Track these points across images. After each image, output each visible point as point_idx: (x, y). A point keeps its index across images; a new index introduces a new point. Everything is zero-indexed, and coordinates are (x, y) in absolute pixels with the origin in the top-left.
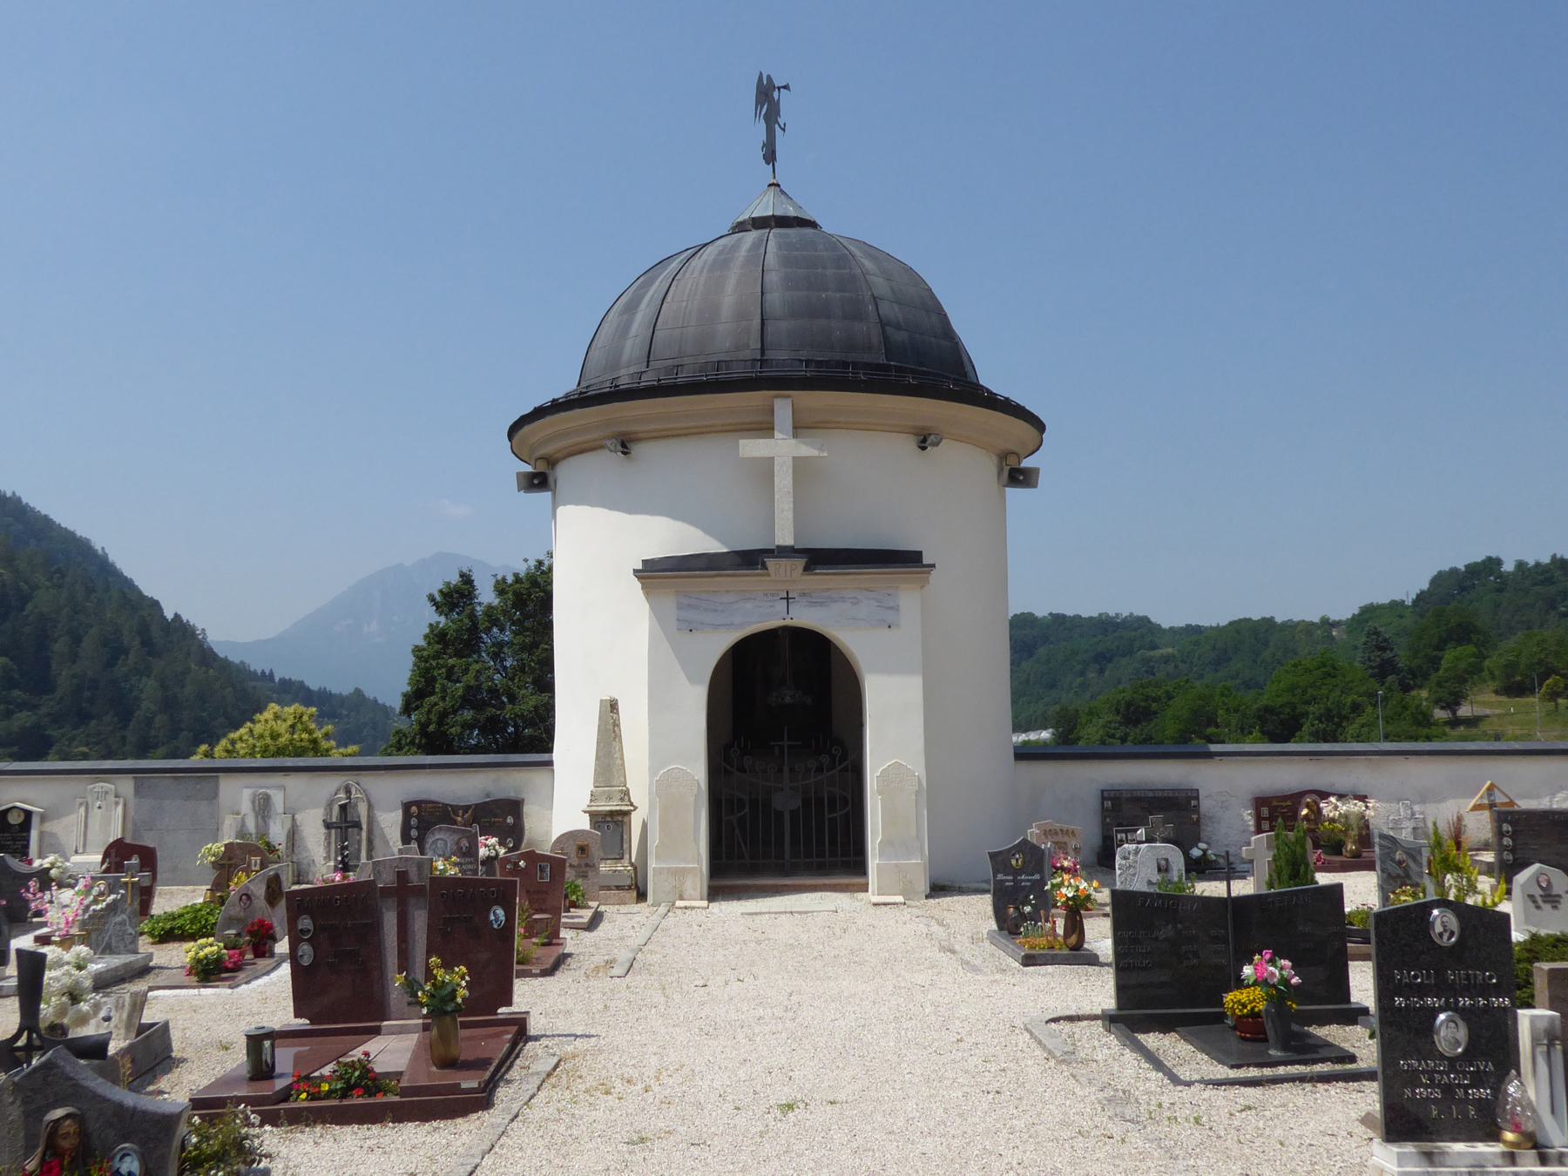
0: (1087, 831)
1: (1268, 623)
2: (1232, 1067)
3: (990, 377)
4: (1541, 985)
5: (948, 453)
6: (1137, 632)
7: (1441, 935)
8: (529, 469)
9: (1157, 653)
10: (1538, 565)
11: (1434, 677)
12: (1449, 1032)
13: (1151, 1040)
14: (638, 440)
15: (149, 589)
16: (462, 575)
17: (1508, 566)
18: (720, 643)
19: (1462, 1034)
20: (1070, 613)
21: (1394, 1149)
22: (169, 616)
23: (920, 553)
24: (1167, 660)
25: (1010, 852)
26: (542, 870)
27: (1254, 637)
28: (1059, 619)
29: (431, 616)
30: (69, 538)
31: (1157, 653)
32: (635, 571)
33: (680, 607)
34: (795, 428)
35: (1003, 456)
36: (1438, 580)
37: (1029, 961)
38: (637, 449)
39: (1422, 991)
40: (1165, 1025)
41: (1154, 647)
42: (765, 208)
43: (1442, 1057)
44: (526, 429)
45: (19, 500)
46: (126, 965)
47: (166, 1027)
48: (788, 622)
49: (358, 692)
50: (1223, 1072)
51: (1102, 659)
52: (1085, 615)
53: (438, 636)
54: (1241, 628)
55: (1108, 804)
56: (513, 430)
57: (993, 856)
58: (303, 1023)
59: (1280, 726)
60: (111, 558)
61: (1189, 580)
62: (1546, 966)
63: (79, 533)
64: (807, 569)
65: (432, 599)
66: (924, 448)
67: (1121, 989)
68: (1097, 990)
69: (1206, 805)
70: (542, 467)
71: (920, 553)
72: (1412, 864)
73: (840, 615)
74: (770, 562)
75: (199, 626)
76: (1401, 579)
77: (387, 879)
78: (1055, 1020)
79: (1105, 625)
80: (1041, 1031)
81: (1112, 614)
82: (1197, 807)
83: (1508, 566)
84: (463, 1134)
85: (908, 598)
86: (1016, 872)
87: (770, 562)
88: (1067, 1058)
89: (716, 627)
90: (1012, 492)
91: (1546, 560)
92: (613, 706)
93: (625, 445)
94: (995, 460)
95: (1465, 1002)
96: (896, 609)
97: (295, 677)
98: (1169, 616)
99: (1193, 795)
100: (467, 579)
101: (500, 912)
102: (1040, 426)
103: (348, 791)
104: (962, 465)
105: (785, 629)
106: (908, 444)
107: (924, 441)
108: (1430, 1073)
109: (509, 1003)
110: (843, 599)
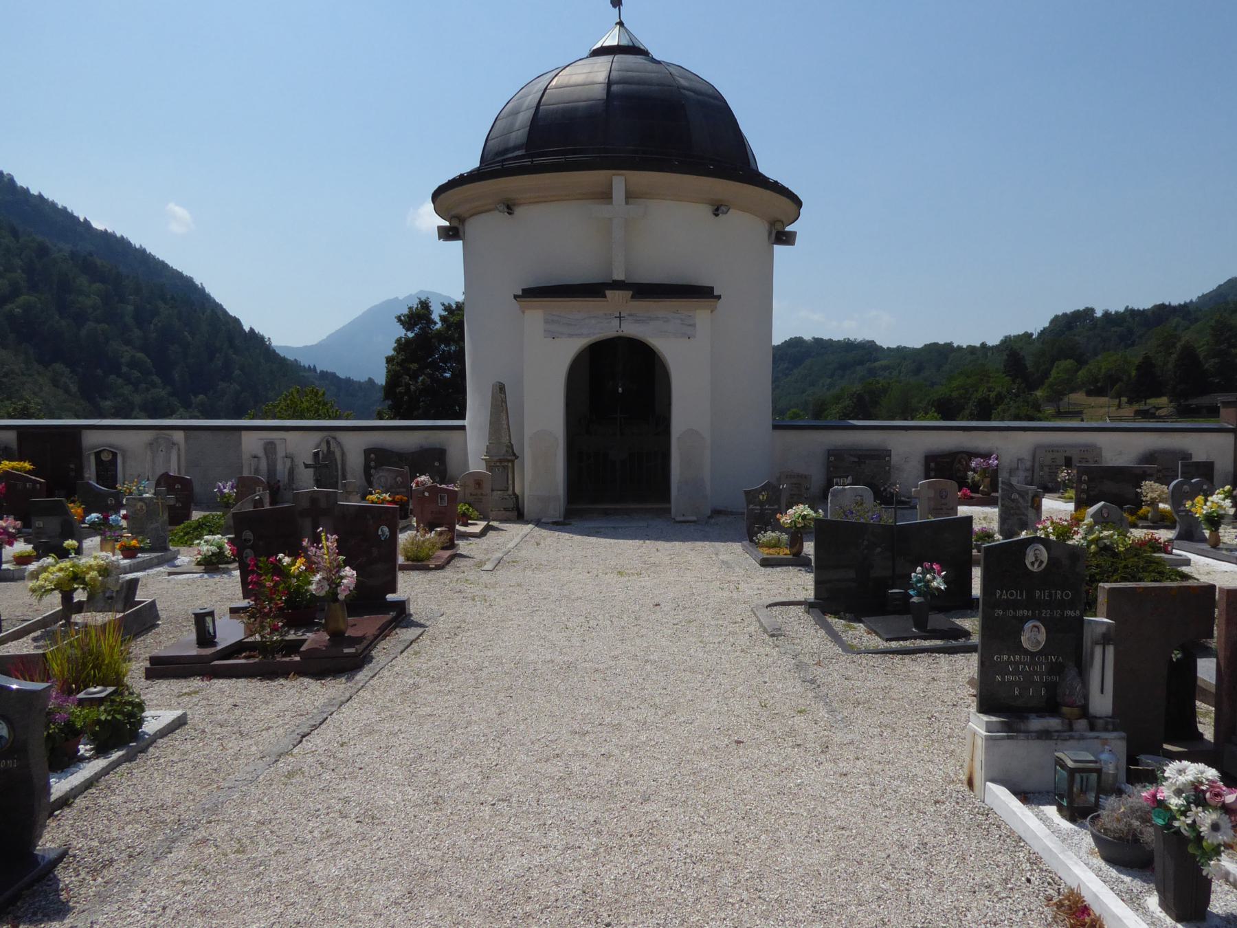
0: (817, 475)
1: (949, 346)
2: (887, 640)
3: (765, 167)
4: (1102, 599)
5: (734, 218)
6: (868, 351)
7: (1033, 564)
8: (447, 224)
9: (877, 364)
10: (1117, 313)
11: (1047, 382)
12: (1033, 636)
13: (832, 620)
14: (520, 205)
15: (232, 311)
16: (421, 302)
17: (1099, 314)
18: (570, 348)
19: (1042, 637)
20: (826, 337)
21: (985, 718)
22: (247, 329)
23: (712, 288)
24: (885, 368)
25: (759, 491)
26: (442, 498)
27: (939, 354)
28: (818, 341)
29: (400, 332)
30: (178, 275)
31: (877, 364)
32: (516, 297)
33: (546, 322)
34: (627, 198)
35: (773, 223)
36: (1056, 320)
37: (766, 563)
38: (519, 211)
39: (1015, 605)
40: (836, 614)
41: (876, 360)
42: (611, 40)
43: (1026, 652)
44: (443, 196)
45: (144, 250)
46: (1037, 449)
47: (153, 604)
48: (620, 334)
49: (370, 379)
50: (883, 645)
51: (844, 367)
52: (835, 339)
53: (402, 346)
54: (932, 349)
55: (832, 458)
56: (436, 196)
57: (747, 493)
58: (244, 603)
59: (947, 409)
60: (207, 290)
61: (896, 318)
62: (1107, 585)
63: (185, 273)
64: (633, 297)
65: (399, 319)
66: (717, 215)
67: (818, 583)
68: (802, 584)
69: (895, 459)
70: (456, 224)
71: (712, 288)
72: (1021, 500)
73: (658, 329)
74: (608, 293)
75: (266, 336)
76: (1033, 320)
77: (305, 504)
78: (771, 605)
79: (849, 347)
80: (763, 614)
81: (852, 339)
82: (889, 461)
83: (1099, 314)
84: (334, 688)
85: (701, 315)
86: (761, 504)
87: (608, 293)
88: (776, 634)
89: (571, 336)
90: (778, 249)
91: (1122, 310)
92: (501, 388)
93: (510, 208)
94: (767, 226)
95: (1046, 613)
96: (694, 325)
97: (330, 369)
98: (887, 341)
99: (888, 453)
100: (425, 305)
101: (386, 529)
102: (798, 203)
103: (328, 443)
104: (743, 225)
105: (620, 338)
106: (705, 211)
107: (717, 209)
108: (1017, 664)
109: (394, 591)
110: (657, 318)
